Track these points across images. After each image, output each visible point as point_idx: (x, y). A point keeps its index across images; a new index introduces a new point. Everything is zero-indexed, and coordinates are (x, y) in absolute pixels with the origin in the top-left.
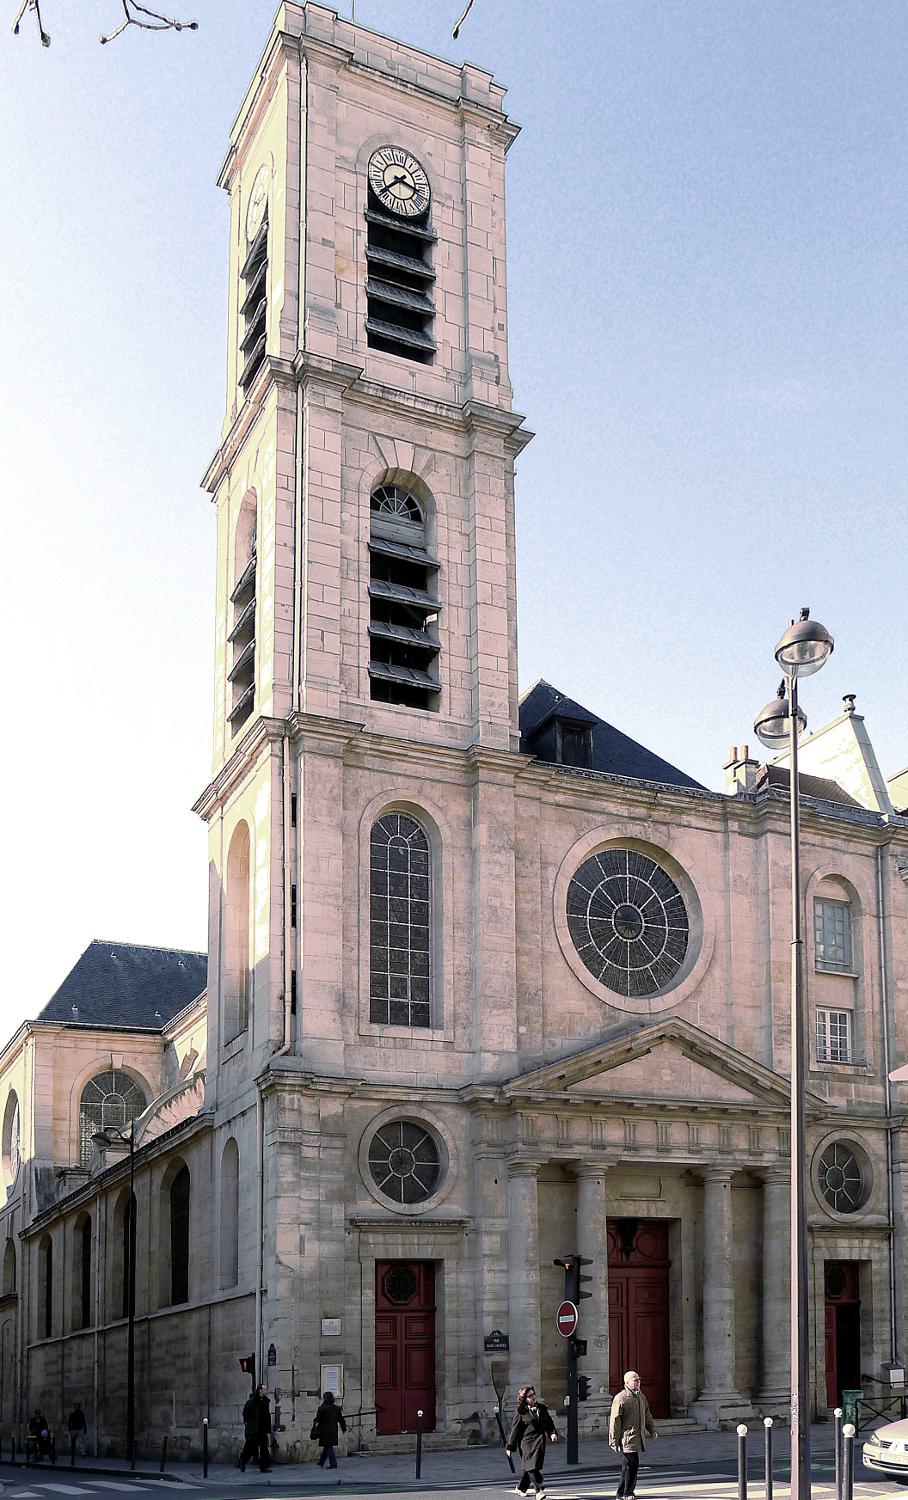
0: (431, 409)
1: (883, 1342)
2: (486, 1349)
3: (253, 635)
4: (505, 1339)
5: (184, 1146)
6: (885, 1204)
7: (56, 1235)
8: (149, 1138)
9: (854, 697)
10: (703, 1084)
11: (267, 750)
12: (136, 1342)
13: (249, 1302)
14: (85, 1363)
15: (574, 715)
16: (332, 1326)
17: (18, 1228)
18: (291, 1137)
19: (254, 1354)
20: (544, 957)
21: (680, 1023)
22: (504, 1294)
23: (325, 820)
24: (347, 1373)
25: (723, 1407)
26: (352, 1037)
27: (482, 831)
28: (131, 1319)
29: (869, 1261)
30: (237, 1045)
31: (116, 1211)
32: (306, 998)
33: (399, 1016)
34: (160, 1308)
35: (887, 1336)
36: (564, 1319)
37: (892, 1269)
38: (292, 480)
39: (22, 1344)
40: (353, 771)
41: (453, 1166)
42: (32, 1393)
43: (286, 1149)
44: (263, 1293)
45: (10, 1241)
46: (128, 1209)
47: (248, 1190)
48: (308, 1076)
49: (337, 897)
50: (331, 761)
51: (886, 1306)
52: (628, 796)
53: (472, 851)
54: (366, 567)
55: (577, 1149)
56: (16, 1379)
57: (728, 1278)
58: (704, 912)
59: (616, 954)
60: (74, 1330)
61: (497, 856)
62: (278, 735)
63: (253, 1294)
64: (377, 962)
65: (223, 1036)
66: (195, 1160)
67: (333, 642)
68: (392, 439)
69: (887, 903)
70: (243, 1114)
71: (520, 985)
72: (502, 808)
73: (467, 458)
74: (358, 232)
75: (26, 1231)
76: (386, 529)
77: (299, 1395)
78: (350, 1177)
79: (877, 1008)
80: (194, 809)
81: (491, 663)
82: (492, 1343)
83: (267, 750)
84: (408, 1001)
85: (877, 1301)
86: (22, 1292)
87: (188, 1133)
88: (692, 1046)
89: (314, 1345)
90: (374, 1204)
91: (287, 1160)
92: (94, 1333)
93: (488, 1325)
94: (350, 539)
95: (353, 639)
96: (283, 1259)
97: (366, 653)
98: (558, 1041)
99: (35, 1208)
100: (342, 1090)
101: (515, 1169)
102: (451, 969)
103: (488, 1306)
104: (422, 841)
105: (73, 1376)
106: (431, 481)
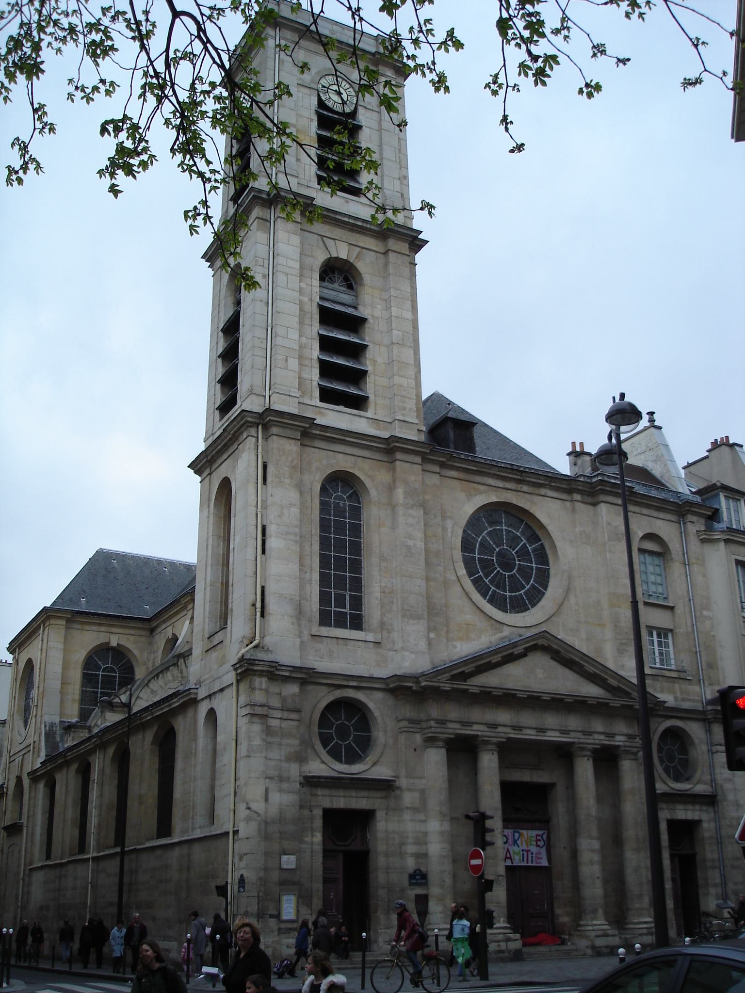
0: (360, 224)
1: (715, 886)
2: (411, 884)
7: (60, 778)
10: (566, 683)
12: (126, 868)
16: (289, 861)
17: (28, 768)
18: (258, 710)
19: (227, 882)
21: (547, 635)
22: (422, 840)
23: (287, 481)
24: (300, 901)
25: (597, 936)
26: (306, 637)
27: (400, 493)
30: (216, 639)
32: (270, 600)
33: (340, 622)
35: (718, 881)
36: (474, 862)
37: (718, 828)
38: (266, 262)
39: (25, 865)
40: (308, 449)
43: (256, 720)
44: (236, 832)
45: (19, 779)
46: (123, 760)
47: (225, 749)
48: (274, 664)
51: (716, 856)
54: (317, 317)
55: (476, 727)
56: (17, 895)
57: (595, 832)
59: (499, 582)
60: (71, 855)
61: (411, 512)
63: (227, 833)
64: (324, 580)
65: (206, 631)
66: (181, 724)
67: (294, 364)
68: (334, 239)
69: (690, 555)
70: (222, 690)
72: (413, 478)
74: (312, 120)
77: (262, 918)
81: (404, 382)
84: (347, 610)
86: (28, 821)
89: (275, 876)
90: (321, 766)
91: (257, 728)
92: (88, 859)
93: (411, 864)
94: (306, 299)
95: (307, 362)
97: (316, 372)
99: (43, 754)
100: (299, 676)
102: (378, 589)
103: (410, 849)
104: (356, 496)
106: (361, 266)
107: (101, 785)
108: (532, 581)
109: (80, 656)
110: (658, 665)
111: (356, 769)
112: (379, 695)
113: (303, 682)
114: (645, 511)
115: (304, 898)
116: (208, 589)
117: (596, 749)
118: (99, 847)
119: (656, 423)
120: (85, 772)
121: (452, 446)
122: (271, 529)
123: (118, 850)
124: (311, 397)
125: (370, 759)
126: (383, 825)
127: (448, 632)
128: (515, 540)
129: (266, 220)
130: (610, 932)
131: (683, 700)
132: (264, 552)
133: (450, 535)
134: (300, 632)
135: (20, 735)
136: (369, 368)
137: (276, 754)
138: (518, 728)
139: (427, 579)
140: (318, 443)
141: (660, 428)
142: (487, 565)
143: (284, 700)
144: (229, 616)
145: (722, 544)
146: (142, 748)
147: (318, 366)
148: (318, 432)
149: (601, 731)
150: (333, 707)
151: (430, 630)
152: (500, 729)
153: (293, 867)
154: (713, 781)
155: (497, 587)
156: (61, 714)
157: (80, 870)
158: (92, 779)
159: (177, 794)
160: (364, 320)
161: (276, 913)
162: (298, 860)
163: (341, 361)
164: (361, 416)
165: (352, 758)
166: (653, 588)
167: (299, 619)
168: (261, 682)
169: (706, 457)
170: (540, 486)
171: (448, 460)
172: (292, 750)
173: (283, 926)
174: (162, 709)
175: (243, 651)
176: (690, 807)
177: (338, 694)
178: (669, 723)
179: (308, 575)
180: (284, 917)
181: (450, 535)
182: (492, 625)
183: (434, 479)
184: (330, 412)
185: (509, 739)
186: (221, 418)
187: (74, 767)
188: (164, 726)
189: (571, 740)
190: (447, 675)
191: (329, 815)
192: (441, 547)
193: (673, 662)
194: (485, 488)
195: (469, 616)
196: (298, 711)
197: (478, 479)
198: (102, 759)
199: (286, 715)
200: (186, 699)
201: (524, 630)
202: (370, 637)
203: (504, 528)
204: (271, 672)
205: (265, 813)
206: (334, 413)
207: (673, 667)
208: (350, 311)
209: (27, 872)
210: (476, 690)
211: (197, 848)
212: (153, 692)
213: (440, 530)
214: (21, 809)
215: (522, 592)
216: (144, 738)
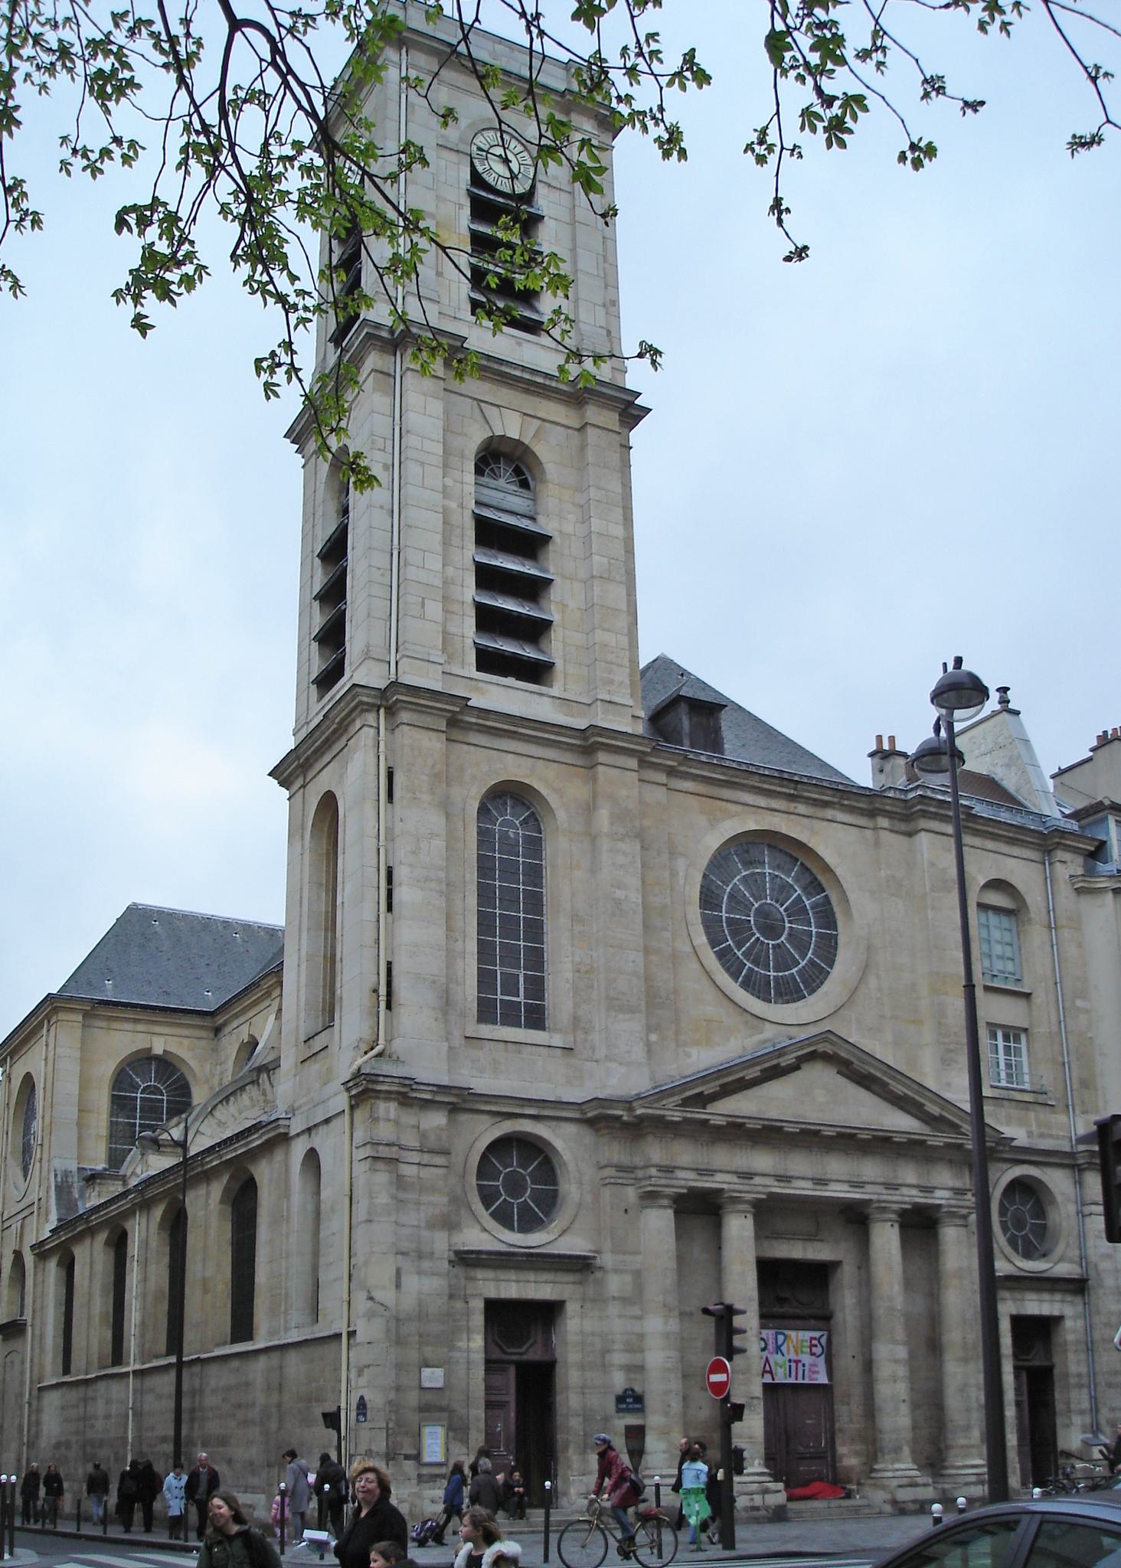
1: (1082, 1412)
2: (619, 1410)
3: (344, 597)
4: (639, 1399)
5: (253, 1155)
6: (1077, 1252)
7: (80, 1252)
8: (208, 1143)
14: (114, 1409)
15: (702, 696)
16: (433, 1377)
17: (31, 1239)
20: (675, 958)
22: (636, 1345)
23: (426, 797)
24: (451, 1434)
25: (900, 1486)
26: (457, 1040)
27: (603, 815)
28: (180, 1358)
30: (318, 1044)
33: (510, 1016)
34: (218, 1345)
36: (716, 1378)
37: (1089, 1328)
39: (31, 1382)
40: (458, 746)
41: (571, 1189)
42: (43, 1442)
43: (380, 1166)
44: (352, 1334)
45: (18, 1256)
46: (176, 1225)
48: (407, 1082)
49: (439, 881)
51: (1083, 1369)
53: (593, 838)
54: (471, 534)
55: (719, 1177)
56: (21, 1426)
57: (900, 1334)
58: (854, 910)
61: (621, 845)
62: (373, 705)
63: (338, 1336)
66: (264, 1173)
68: (498, 406)
70: (327, 1121)
72: (624, 793)
73: (579, 430)
74: (461, 206)
79: (1054, 1028)
81: (610, 639)
84: (521, 999)
85: (1071, 1363)
87: (256, 1140)
88: (847, 1063)
89: (413, 1398)
90: (484, 1234)
91: (382, 1178)
92: (127, 1374)
93: (619, 1382)
96: (375, 1294)
97: (471, 622)
98: (746, 1234)
101: (650, 1197)
102: (569, 966)
105: (99, 1424)
106: (541, 450)
107: (145, 1263)
108: (810, 955)
109: (107, 1069)
110: (1003, 1084)
111: (534, 1240)
112: (571, 1129)
113: (454, 1109)
117: (905, 1211)
118: (144, 1356)
119: (1010, 706)
120: (119, 1243)
121: (686, 741)
122: (401, 874)
123: (173, 1359)
125: (556, 1226)
127: (677, 1033)
129: (389, 375)
130: (920, 1480)
131: (1041, 1136)
132: (390, 908)
133: (682, 882)
139: (647, 951)
140: (475, 738)
142: (739, 929)
143: (423, 1136)
144: (337, 1009)
145: (1110, 895)
147: (473, 613)
148: (474, 720)
150: (500, 1146)
151: (649, 1029)
152: (757, 1180)
153: (440, 1384)
154: (1083, 1258)
155: (756, 962)
156: (80, 1158)
157: (115, 1388)
161: (414, 1452)
162: (447, 1376)
164: (542, 694)
165: (529, 1222)
166: (999, 965)
167: (445, 1013)
169: (1090, 760)
170: (826, 805)
171: (680, 764)
172: (437, 1211)
173: (425, 1471)
174: (235, 1150)
175: (360, 1061)
176: (1046, 1296)
178: (1017, 1171)
180: (427, 1458)
181: (682, 882)
182: (746, 1023)
185: (771, 1195)
187: (102, 1236)
189: (867, 1197)
190: (676, 1098)
191: (495, 1309)
192: (668, 901)
195: (711, 1008)
196: (446, 1152)
199: (426, 1158)
200: (272, 1134)
202: (557, 1040)
205: (397, 1305)
206: (501, 689)
207: (1027, 1086)
208: (524, 523)
209: (35, 1392)
210: (720, 1121)
212: (221, 1124)
213: (667, 874)
215: (794, 971)
216: (208, 1193)
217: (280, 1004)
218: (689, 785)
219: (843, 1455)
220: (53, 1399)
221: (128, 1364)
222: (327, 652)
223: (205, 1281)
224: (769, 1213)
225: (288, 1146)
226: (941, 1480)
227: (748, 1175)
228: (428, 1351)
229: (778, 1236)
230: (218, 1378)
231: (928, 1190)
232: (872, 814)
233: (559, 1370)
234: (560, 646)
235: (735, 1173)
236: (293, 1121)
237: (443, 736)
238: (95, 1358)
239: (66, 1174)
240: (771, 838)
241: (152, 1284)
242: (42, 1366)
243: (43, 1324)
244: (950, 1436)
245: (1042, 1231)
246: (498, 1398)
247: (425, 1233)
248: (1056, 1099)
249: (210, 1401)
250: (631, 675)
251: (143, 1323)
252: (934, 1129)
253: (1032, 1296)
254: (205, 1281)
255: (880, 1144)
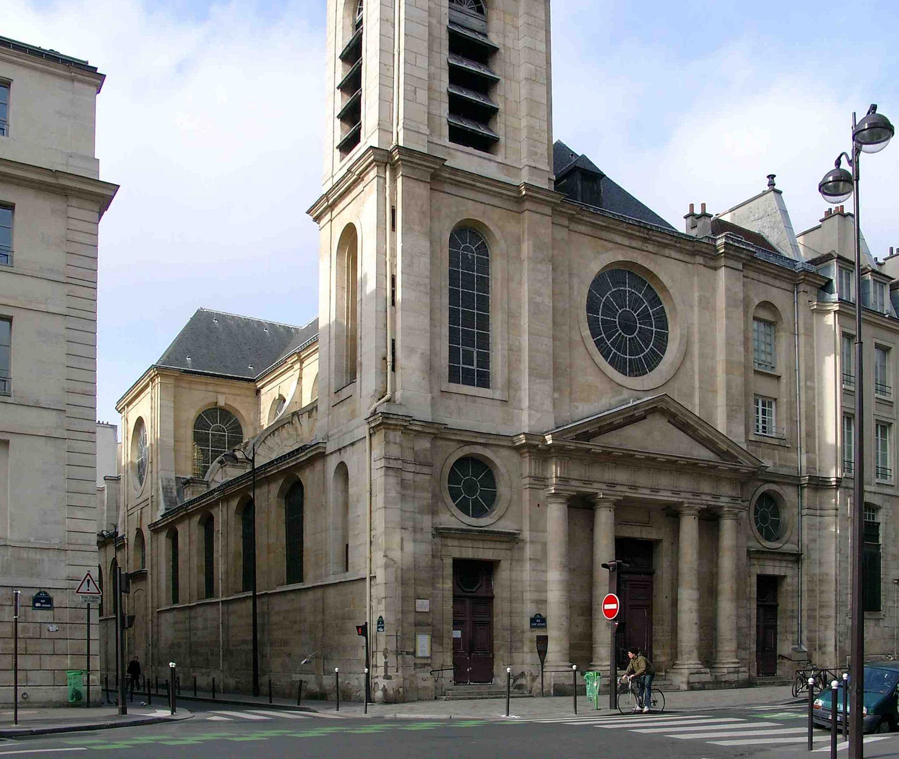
1: (793, 633)
2: (531, 627)
4: (544, 620)
5: (300, 467)
7: (181, 529)
9: (774, 176)
11: (373, 173)
13: (361, 584)
16: (423, 605)
17: (147, 521)
18: (393, 464)
20: (571, 345)
23: (417, 228)
26: (436, 393)
28: (254, 593)
29: (785, 576)
30: (345, 393)
31: (237, 512)
33: (468, 379)
34: (278, 585)
35: (795, 629)
42: (162, 644)
43: (391, 472)
44: (373, 578)
45: (139, 532)
46: (247, 510)
50: (422, 185)
52: (629, 231)
54: (446, 43)
55: (596, 485)
56: (147, 634)
66: (308, 478)
70: (352, 444)
71: (555, 363)
75: (156, 523)
76: (460, 17)
78: (434, 496)
80: (308, 212)
82: (535, 622)
83: (373, 173)
84: (475, 367)
85: (786, 603)
89: (411, 618)
94: (434, 22)
97: (445, 106)
104: (484, 249)
105: (200, 633)
107: (226, 535)
109: (191, 415)
110: (760, 432)
112: (505, 453)
113: (435, 437)
114: (762, 278)
115: (437, 639)
116: (333, 343)
117: (702, 509)
118: (226, 592)
119: (775, 187)
120: (208, 523)
121: (579, 198)
123: (250, 594)
124: (440, 136)
125: (496, 514)
126: (503, 576)
127: (571, 393)
128: (637, 302)
130: (703, 670)
131: (781, 466)
133: (576, 293)
134: (431, 388)
135: (136, 489)
136: (501, 106)
137: (410, 506)
138: (634, 487)
139: (554, 338)
140: (448, 188)
141: (780, 192)
142: (609, 328)
143: (416, 454)
144: (358, 370)
146: (269, 501)
148: (447, 176)
149: (708, 493)
150: (462, 462)
151: (556, 389)
152: (618, 488)
153: (427, 610)
154: (799, 542)
155: (618, 349)
156: (176, 471)
157: (210, 612)
158: (216, 529)
159: (308, 542)
160: (495, 50)
162: (432, 603)
163: (471, 96)
164: (490, 160)
165: (479, 512)
166: (763, 357)
168: (396, 436)
169: (820, 227)
170: (666, 246)
171: (578, 213)
172: (425, 503)
173: (419, 661)
174: (288, 463)
175: (376, 404)
176: (777, 563)
177: (467, 450)
178: (766, 487)
179: (437, 330)
180: (419, 654)
183: (563, 234)
184: (460, 154)
185: (626, 498)
186: (342, 159)
187: (197, 518)
188: (291, 478)
189: (681, 500)
193: (774, 430)
194: (610, 245)
196: (430, 465)
197: (604, 234)
198: (225, 512)
200: (315, 453)
201: (642, 393)
202: (498, 395)
203: (628, 289)
204: (405, 426)
206: (466, 156)
207: (774, 435)
208: (480, 38)
209: (155, 614)
210: (598, 450)
211: (331, 592)
212: (271, 449)
213: (567, 286)
214: (143, 558)
215: (641, 356)
216: (269, 491)
217: (301, 374)
218: (582, 228)
219: (657, 655)
220: (169, 617)
221: (218, 597)
222: (347, 127)
223: (269, 546)
224: (623, 508)
225: (325, 461)
226: (713, 670)
227: (612, 485)
228: (420, 589)
229: (627, 523)
230: (280, 605)
231: (716, 497)
232: (693, 254)
233: (496, 601)
234: (502, 126)
235: (604, 483)
236: (328, 444)
237: (428, 186)
238: (195, 593)
239: (169, 480)
240: (631, 266)
241: (232, 548)
242: (159, 598)
243: (158, 573)
244: (720, 645)
245: (776, 524)
246: (460, 619)
247: (418, 516)
248: (791, 443)
249: (274, 619)
250: (548, 149)
251: (227, 572)
252: (722, 459)
253: (770, 563)
254: (269, 546)
255: (692, 468)
